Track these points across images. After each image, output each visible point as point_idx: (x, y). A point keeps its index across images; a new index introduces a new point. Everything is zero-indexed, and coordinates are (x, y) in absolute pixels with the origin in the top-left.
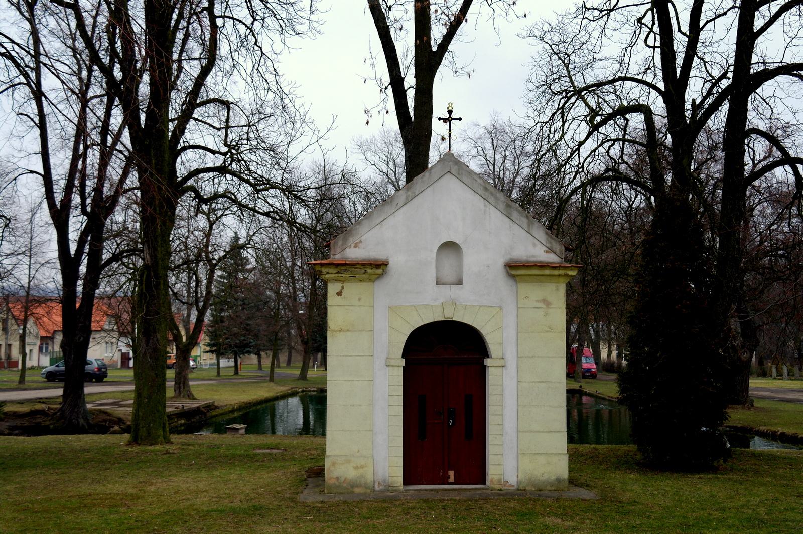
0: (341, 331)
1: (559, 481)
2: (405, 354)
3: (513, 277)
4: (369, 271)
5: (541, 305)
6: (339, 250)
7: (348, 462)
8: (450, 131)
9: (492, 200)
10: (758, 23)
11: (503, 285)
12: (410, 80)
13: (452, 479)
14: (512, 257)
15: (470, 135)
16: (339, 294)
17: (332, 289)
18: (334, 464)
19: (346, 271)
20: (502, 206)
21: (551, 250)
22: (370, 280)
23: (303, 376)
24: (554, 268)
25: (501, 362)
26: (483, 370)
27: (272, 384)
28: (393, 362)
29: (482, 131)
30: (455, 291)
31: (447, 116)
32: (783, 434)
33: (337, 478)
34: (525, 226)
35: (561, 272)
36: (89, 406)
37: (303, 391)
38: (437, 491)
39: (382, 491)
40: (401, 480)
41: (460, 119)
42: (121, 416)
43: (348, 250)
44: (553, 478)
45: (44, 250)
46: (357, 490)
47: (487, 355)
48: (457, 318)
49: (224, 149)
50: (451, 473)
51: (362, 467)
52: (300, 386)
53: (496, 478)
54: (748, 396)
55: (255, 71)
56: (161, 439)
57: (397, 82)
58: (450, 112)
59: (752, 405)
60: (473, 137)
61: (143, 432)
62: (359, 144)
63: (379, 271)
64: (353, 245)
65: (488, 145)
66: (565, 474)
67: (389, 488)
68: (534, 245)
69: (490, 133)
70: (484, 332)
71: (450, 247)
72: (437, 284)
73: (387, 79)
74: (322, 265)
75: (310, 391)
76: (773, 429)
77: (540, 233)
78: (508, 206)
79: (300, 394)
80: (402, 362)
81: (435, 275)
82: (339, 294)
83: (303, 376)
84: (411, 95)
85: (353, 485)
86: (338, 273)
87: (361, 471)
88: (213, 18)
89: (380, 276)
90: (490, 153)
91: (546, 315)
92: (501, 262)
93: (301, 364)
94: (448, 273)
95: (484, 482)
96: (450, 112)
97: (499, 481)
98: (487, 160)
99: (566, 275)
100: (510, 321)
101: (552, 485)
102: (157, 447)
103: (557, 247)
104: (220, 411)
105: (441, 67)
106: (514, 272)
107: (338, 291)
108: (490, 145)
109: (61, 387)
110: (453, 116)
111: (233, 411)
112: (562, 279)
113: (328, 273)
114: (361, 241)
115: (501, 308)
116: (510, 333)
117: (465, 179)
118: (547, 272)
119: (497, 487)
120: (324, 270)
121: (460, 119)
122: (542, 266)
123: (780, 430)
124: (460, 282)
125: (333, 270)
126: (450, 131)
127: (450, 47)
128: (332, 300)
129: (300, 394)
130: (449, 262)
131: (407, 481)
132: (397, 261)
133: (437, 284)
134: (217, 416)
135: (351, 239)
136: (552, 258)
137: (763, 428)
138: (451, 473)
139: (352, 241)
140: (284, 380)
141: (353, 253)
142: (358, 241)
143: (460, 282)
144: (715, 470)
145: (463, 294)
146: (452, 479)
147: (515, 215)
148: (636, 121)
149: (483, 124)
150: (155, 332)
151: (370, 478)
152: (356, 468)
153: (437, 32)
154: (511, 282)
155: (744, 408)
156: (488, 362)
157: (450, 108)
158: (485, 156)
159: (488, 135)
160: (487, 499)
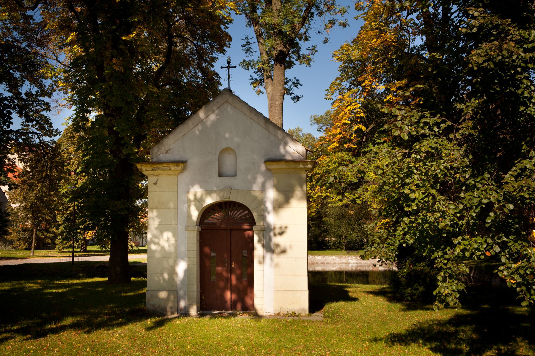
8: (229, 75)
14: (270, 157)
31: (227, 65)
33: (153, 305)
40: (305, 304)
41: (222, 67)
45: (302, 157)
58: (229, 63)
64: (164, 152)
81: (218, 170)
86: (153, 170)
96: (229, 63)
107: (155, 182)
109: (109, 254)
110: (231, 65)
113: (146, 170)
114: (170, 149)
121: (222, 67)
126: (229, 75)
133: (236, 175)
135: (163, 148)
142: (168, 149)
157: (229, 60)
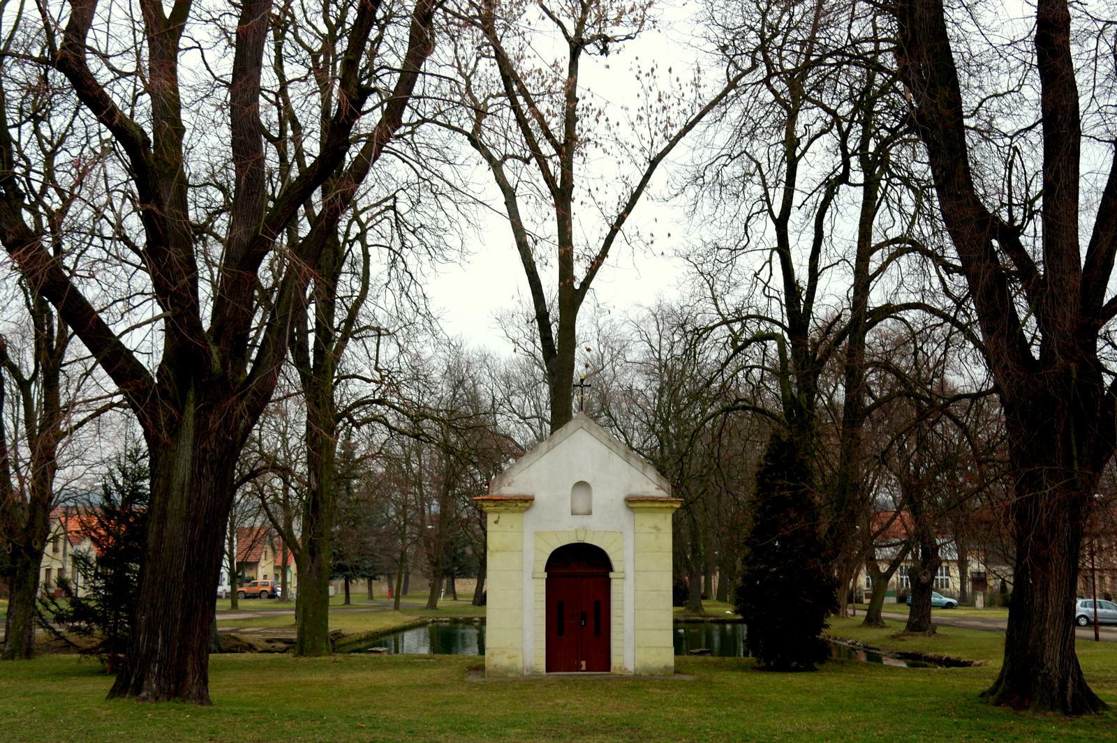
0: (497, 551)
1: (666, 668)
2: (546, 570)
3: (631, 508)
4: (519, 505)
5: (653, 531)
6: (496, 488)
7: (504, 653)
9: (614, 448)
10: (873, 267)
11: (624, 516)
12: (554, 313)
13: (584, 667)
15: (632, 316)
16: (496, 522)
17: (491, 518)
18: (492, 655)
19: (501, 505)
20: (622, 453)
21: (660, 488)
22: (520, 512)
23: (432, 605)
24: (663, 502)
25: (622, 575)
26: (609, 580)
27: (397, 613)
28: (538, 576)
29: (645, 313)
30: (586, 520)
32: (948, 659)
33: (495, 666)
34: (640, 468)
35: (668, 505)
36: (219, 629)
37: (433, 622)
38: (571, 676)
39: (529, 676)
42: (251, 642)
43: (503, 488)
44: (662, 665)
46: (510, 675)
47: (611, 569)
48: (588, 541)
49: (377, 376)
50: (583, 663)
51: (514, 657)
52: (430, 616)
53: (618, 666)
54: (930, 622)
55: (404, 296)
56: (325, 651)
57: (542, 316)
59: (934, 632)
60: (635, 319)
61: (308, 645)
62: (499, 317)
63: (527, 505)
65: (653, 328)
66: (672, 663)
67: (535, 673)
68: (648, 484)
69: (655, 315)
70: (608, 552)
71: (582, 485)
72: (573, 514)
73: (533, 312)
74: (483, 500)
75: (442, 621)
76: (940, 654)
77: (652, 473)
78: (627, 453)
79: (430, 625)
80: (545, 575)
82: (496, 522)
83: (432, 605)
84: (554, 329)
85: (508, 670)
87: (513, 660)
88: (365, 248)
89: (527, 509)
90: (655, 338)
91: (657, 538)
92: (622, 497)
93: (428, 592)
94: (581, 506)
95: (609, 670)
97: (620, 668)
98: (651, 346)
99: (672, 507)
100: (629, 542)
101: (661, 671)
102: (323, 658)
103: (666, 485)
104: (347, 640)
105: (583, 303)
106: (631, 505)
108: (654, 329)
111: (360, 641)
112: (669, 511)
115: (621, 533)
116: (629, 552)
117: (593, 433)
118: (657, 505)
119: (619, 672)
120: (485, 504)
122: (654, 500)
123: (946, 655)
124: (590, 513)
125: (491, 504)
127: (591, 286)
128: (491, 527)
129: (430, 625)
130: (581, 496)
131: (549, 669)
132: (541, 496)
133: (573, 514)
134: (344, 645)
136: (662, 494)
137: (931, 654)
138: (583, 663)
139: (505, 481)
140: (409, 610)
141: (507, 491)
143: (590, 513)
144: (813, 670)
145: (593, 522)
146: (584, 667)
147: (633, 460)
148: (773, 346)
149: (646, 304)
150: (319, 552)
151: (520, 665)
152: (509, 657)
153: (580, 271)
154: (629, 513)
155: (924, 635)
156: (612, 575)
158: (649, 342)
159: (652, 317)
160: (609, 680)
